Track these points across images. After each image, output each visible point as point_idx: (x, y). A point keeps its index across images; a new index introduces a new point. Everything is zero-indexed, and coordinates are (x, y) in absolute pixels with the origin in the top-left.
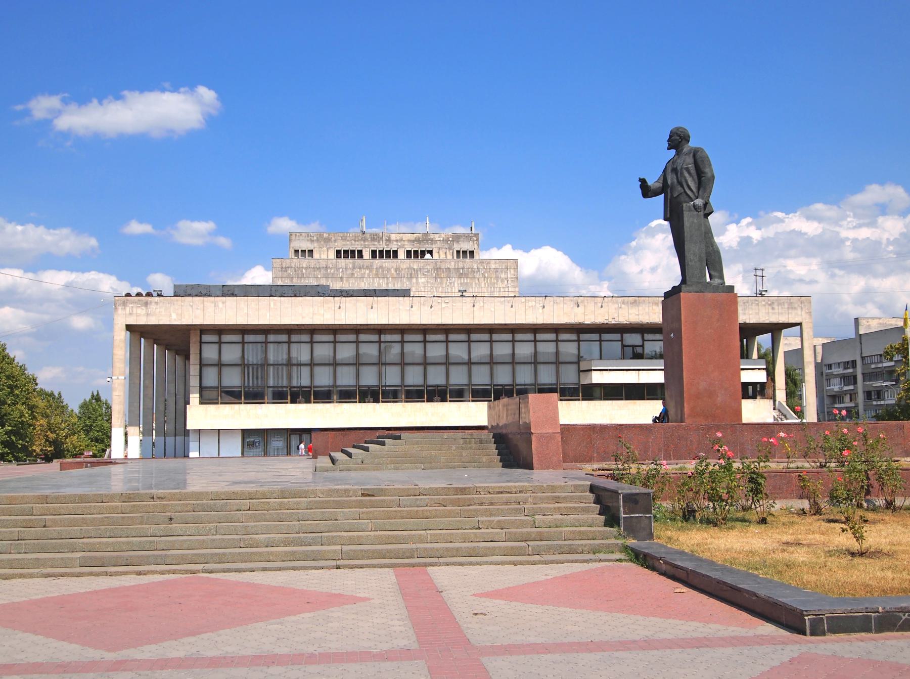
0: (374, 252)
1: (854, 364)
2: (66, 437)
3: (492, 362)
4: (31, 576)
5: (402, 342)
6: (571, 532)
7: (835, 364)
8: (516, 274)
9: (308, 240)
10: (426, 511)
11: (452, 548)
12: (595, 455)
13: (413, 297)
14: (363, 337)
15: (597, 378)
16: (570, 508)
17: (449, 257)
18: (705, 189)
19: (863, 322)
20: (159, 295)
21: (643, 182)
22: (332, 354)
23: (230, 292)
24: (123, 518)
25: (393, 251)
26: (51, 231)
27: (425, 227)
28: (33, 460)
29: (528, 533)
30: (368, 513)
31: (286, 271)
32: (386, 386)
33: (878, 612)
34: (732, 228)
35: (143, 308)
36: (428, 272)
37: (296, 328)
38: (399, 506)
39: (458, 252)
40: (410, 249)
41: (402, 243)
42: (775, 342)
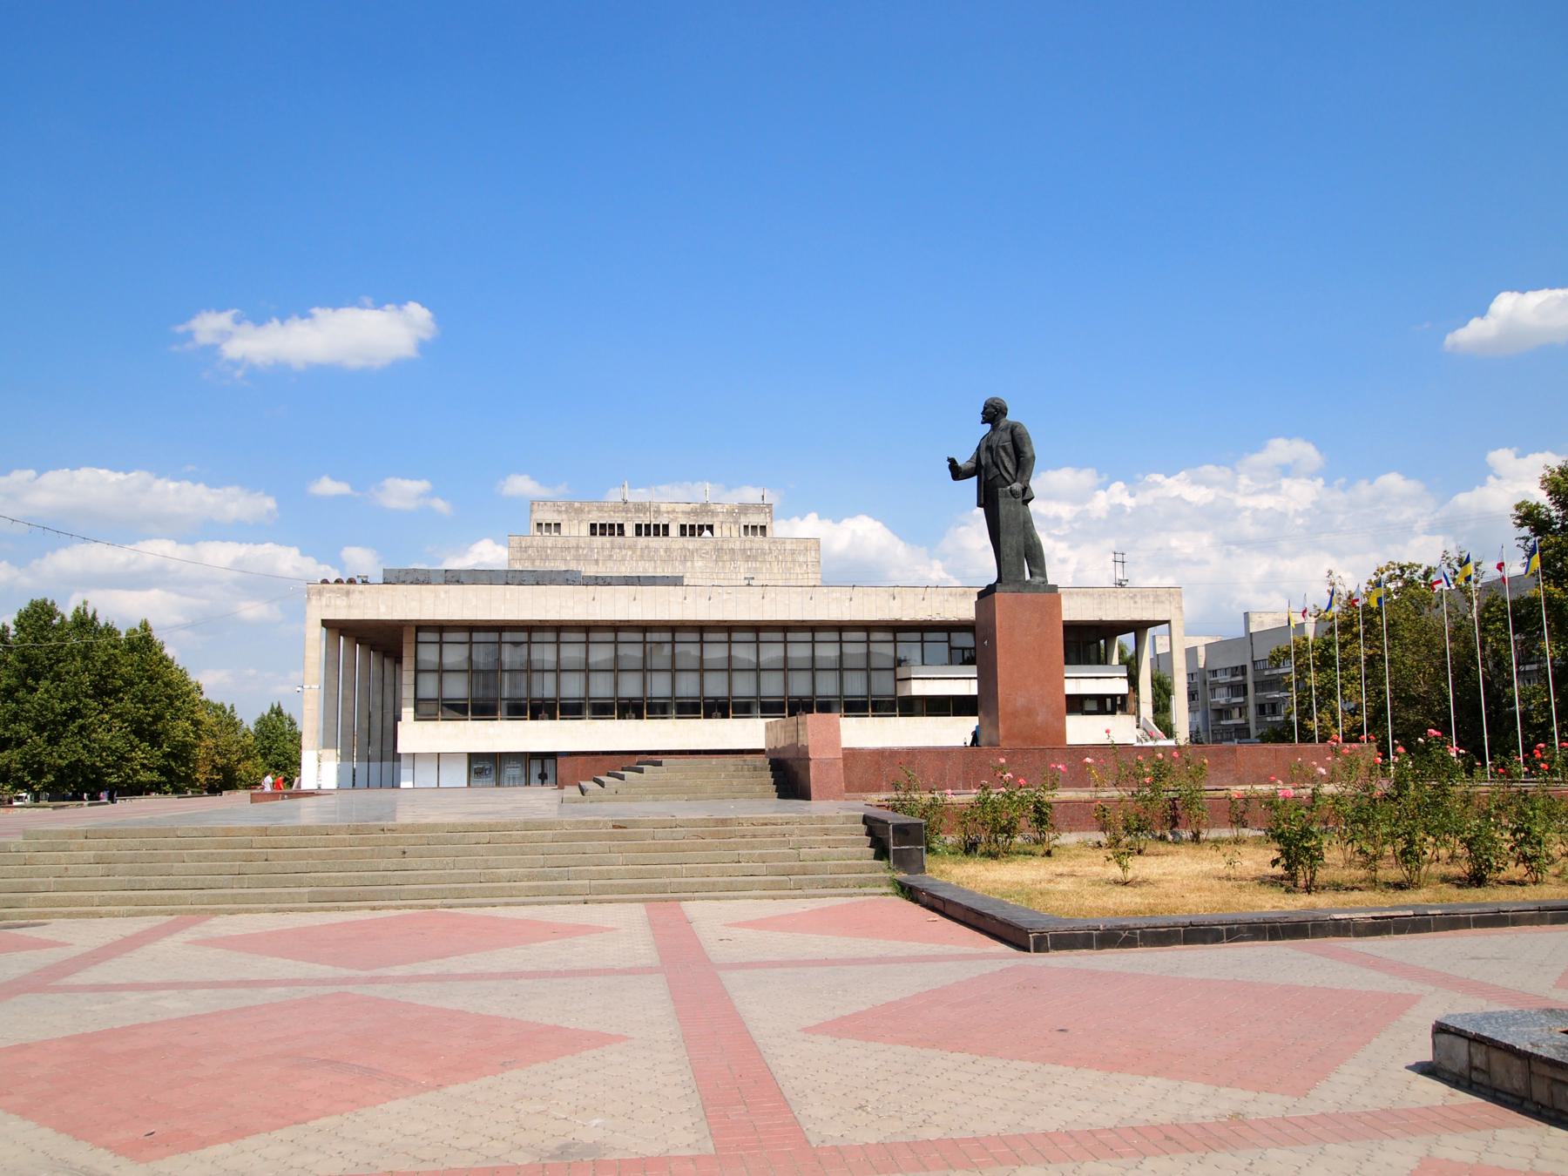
0: (638, 527)
1: (1243, 670)
2: (239, 761)
3: (786, 668)
4: (258, 911)
5: (673, 642)
6: (837, 865)
7: (1220, 669)
8: (817, 556)
10: (683, 844)
11: (708, 883)
12: (884, 784)
13: (687, 585)
14: (623, 636)
15: (918, 688)
16: (840, 840)
17: (735, 534)
18: (1024, 472)
19: (1254, 618)
20: (364, 582)
21: (952, 462)
22: (584, 656)
23: (454, 580)
24: (352, 851)
25: (663, 525)
26: (214, 491)
27: (705, 492)
28: (198, 792)
29: (793, 867)
30: (620, 846)
32: (651, 698)
33: (1098, 930)
34: (1101, 494)
35: (344, 598)
36: (707, 553)
37: (539, 624)
38: (654, 839)
39: (746, 527)
40: (685, 523)
41: (675, 515)
42: (1138, 642)
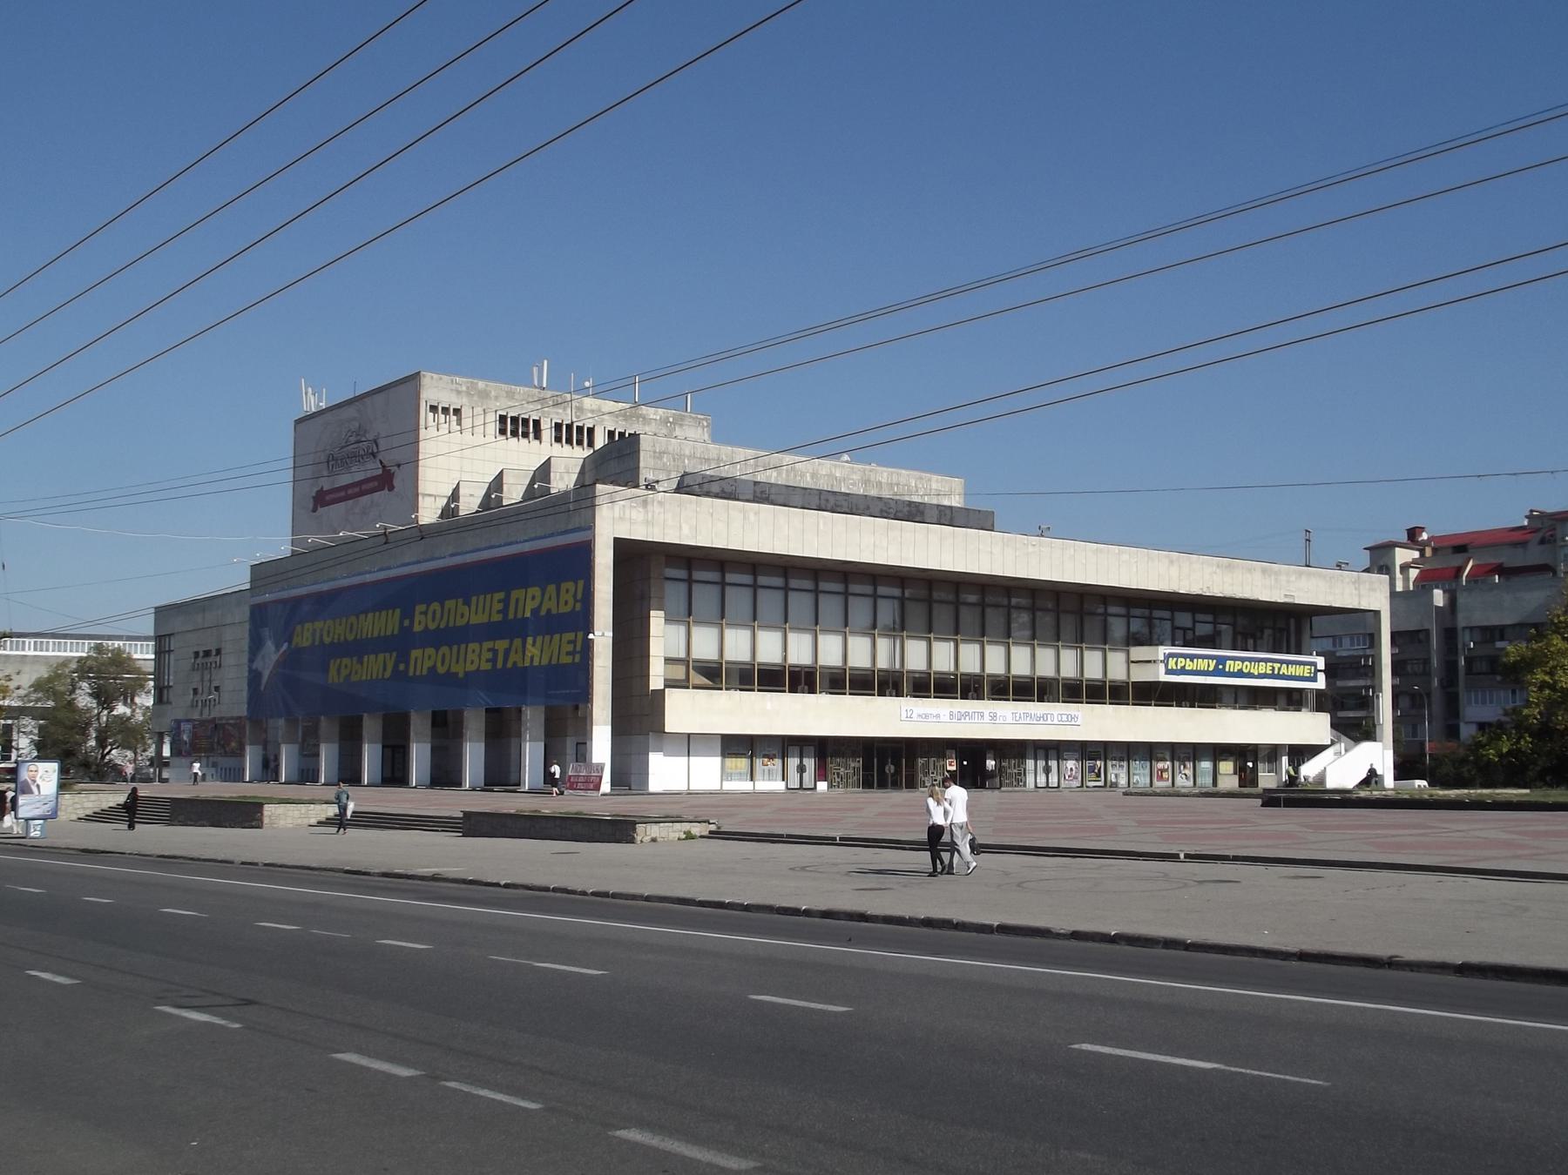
9: (452, 390)
31: (660, 458)
